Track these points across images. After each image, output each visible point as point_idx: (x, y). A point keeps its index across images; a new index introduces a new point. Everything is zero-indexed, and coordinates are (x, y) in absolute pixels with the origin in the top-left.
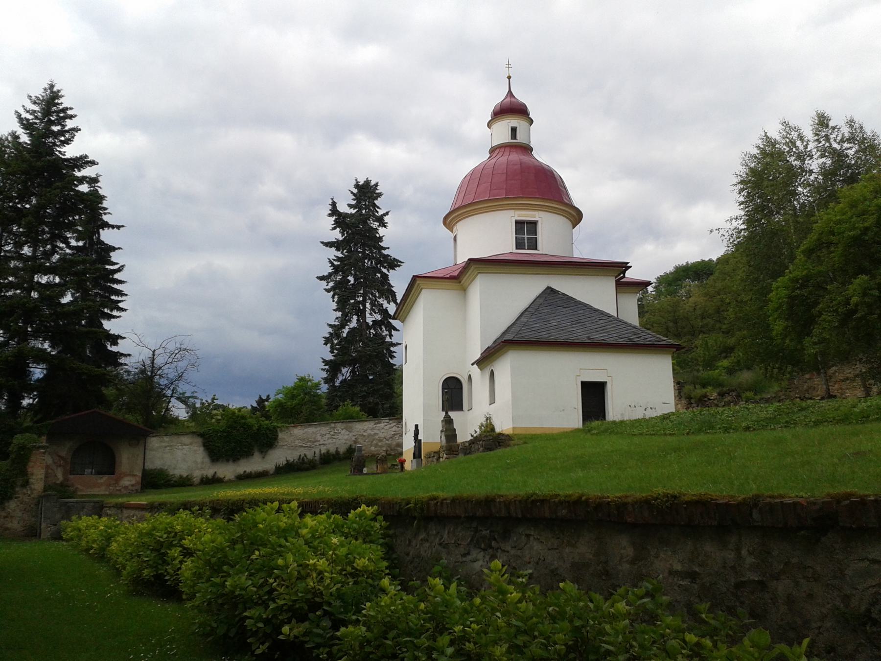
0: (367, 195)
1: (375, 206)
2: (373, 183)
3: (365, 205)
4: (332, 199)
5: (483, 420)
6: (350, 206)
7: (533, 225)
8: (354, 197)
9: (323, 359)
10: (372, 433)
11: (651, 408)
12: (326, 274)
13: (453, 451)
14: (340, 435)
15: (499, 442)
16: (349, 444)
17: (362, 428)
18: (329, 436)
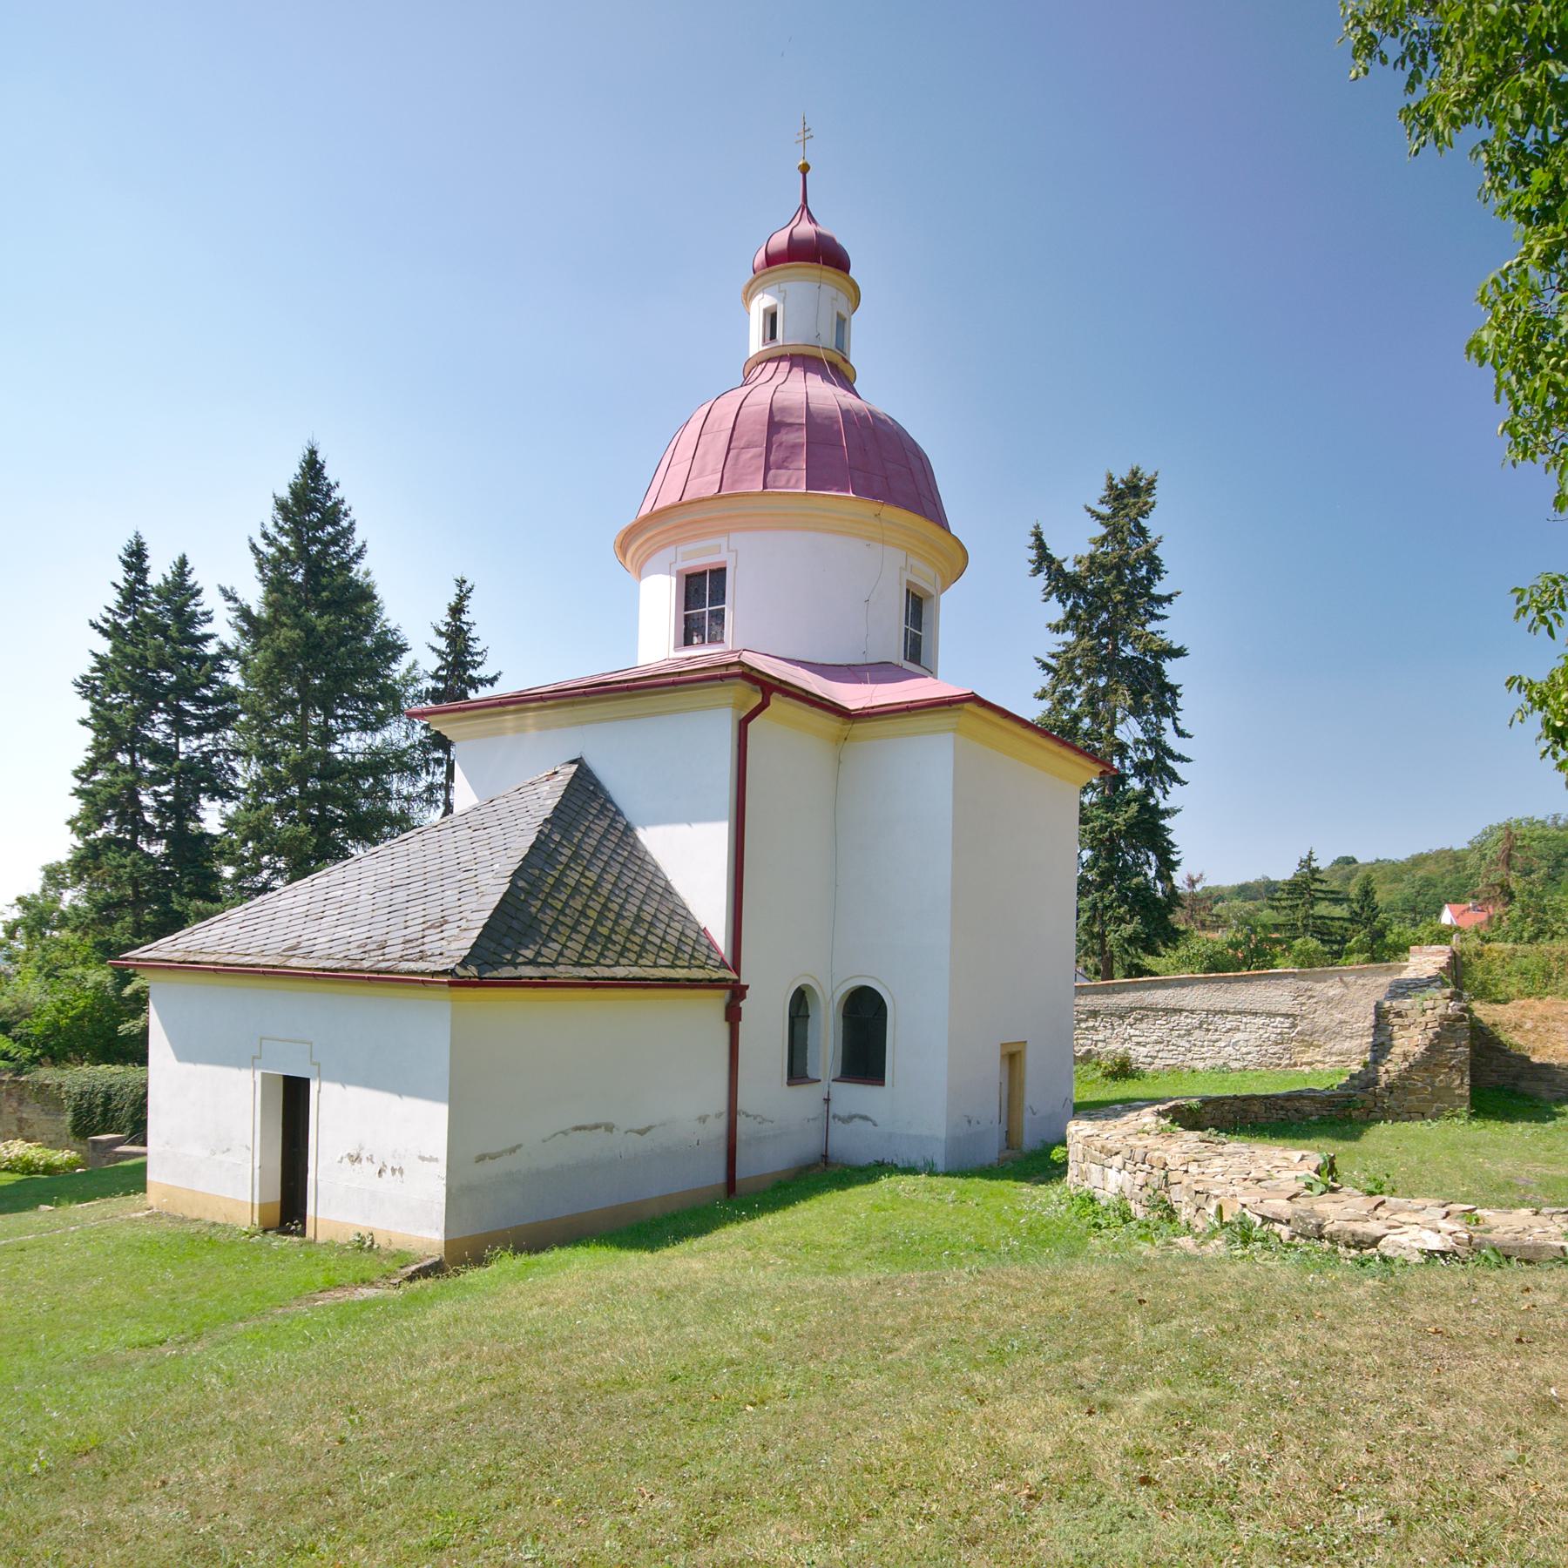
11: (393, 1170)
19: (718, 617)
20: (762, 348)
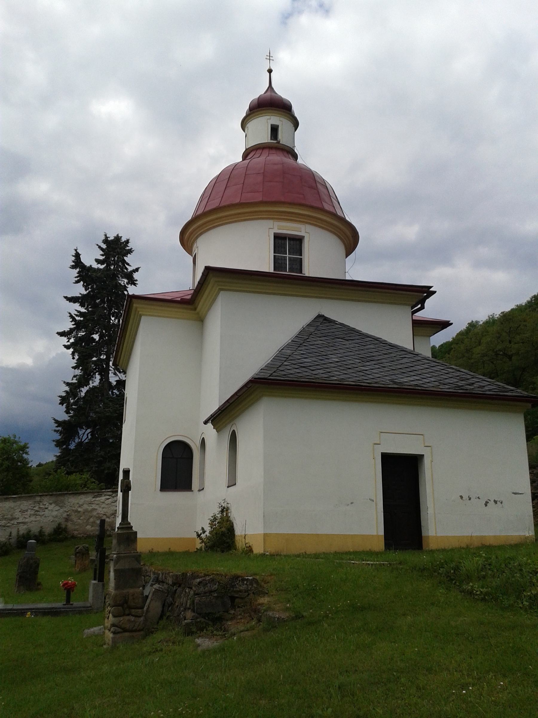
0: (116, 251)
1: (124, 262)
2: (123, 239)
3: (114, 260)
4: (76, 250)
5: (216, 510)
6: (98, 261)
7: (298, 242)
8: (102, 253)
9: (54, 419)
10: (90, 508)
11: (496, 502)
12: (67, 329)
13: (130, 608)
14: (46, 510)
15: (233, 599)
16: (58, 522)
17: (76, 502)
18: (33, 512)
20: (269, 141)
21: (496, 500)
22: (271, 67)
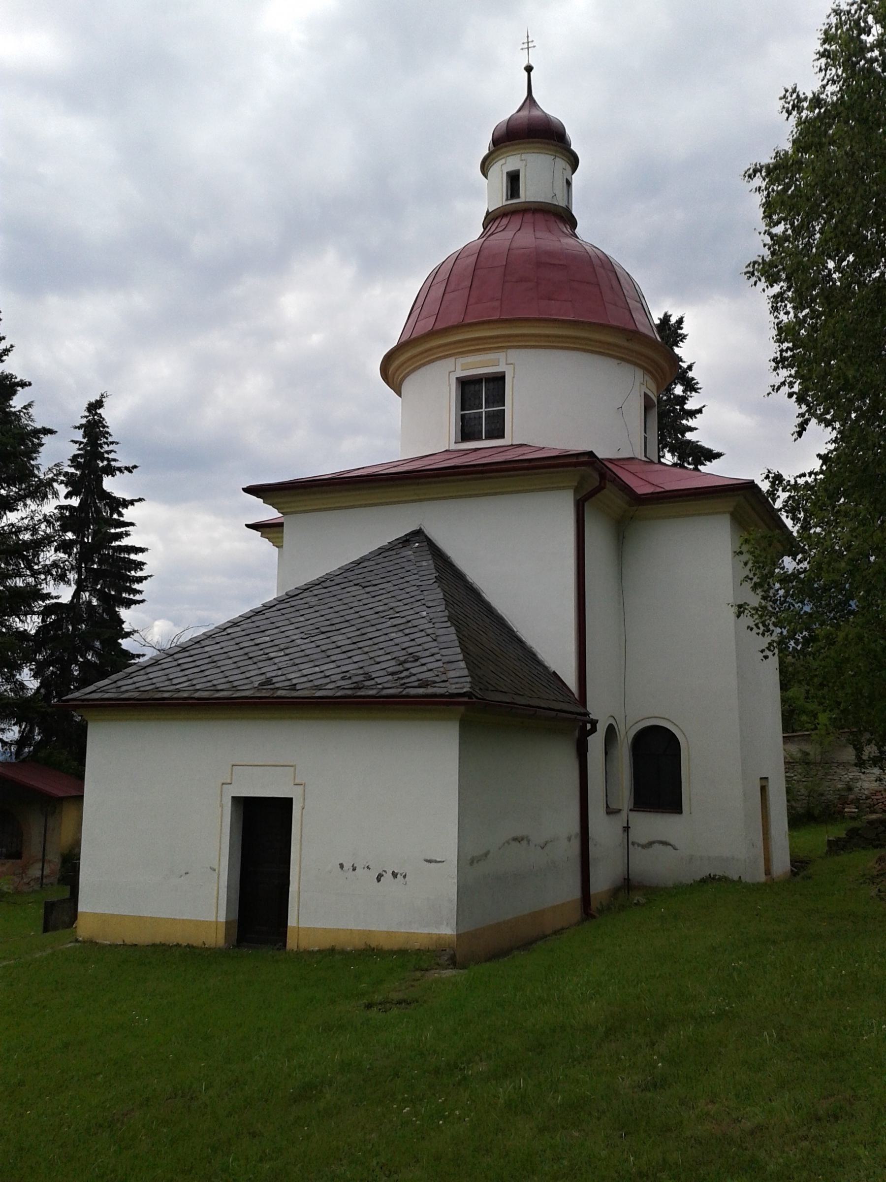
11: (395, 875)
19: (500, 417)
20: (505, 203)
21: (396, 871)
22: (530, 62)
